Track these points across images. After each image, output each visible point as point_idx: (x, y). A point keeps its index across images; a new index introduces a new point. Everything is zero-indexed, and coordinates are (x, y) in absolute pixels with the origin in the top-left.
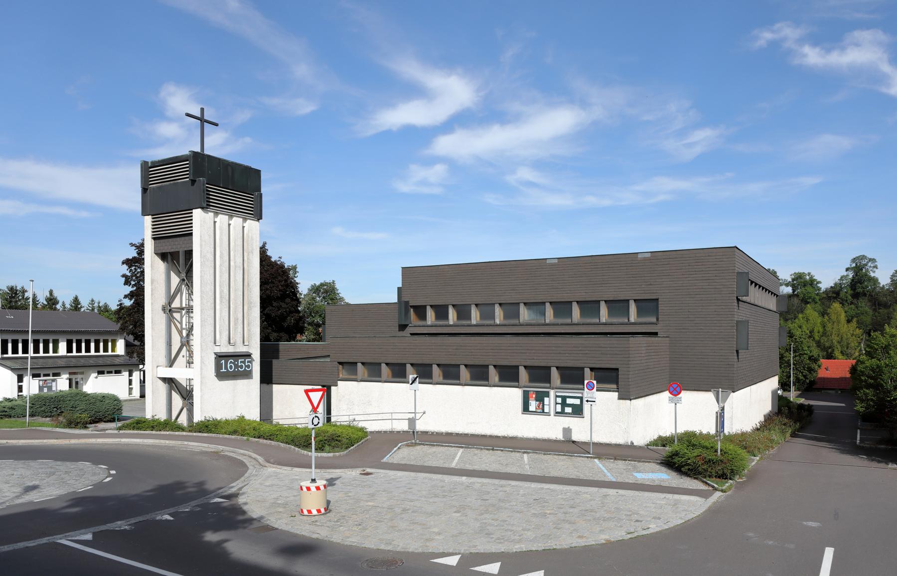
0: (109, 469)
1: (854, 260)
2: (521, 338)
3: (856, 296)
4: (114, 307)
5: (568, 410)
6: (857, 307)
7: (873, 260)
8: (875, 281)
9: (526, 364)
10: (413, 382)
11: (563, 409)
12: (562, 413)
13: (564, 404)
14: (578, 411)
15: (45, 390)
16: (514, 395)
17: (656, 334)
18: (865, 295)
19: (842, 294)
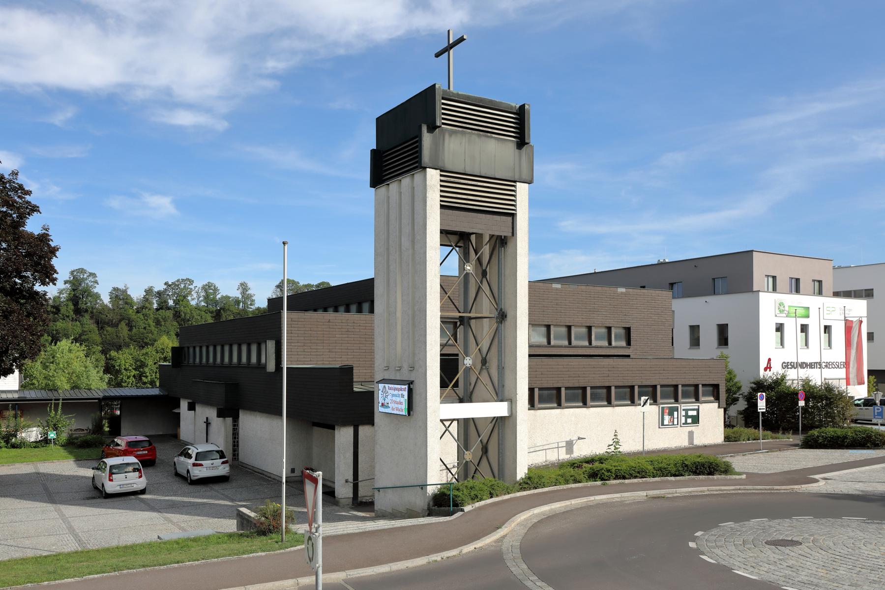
0: (698, 551)
1: (72, 273)
2: (616, 359)
3: (78, 311)
4: (249, 292)
5: (689, 420)
6: (82, 325)
7: (93, 275)
8: (97, 296)
9: (704, 383)
10: (644, 404)
11: (686, 420)
12: (686, 423)
13: (687, 416)
14: (696, 420)
15: (612, 448)
16: (651, 411)
17: (628, 356)
18: (86, 311)
19: (63, 310)
